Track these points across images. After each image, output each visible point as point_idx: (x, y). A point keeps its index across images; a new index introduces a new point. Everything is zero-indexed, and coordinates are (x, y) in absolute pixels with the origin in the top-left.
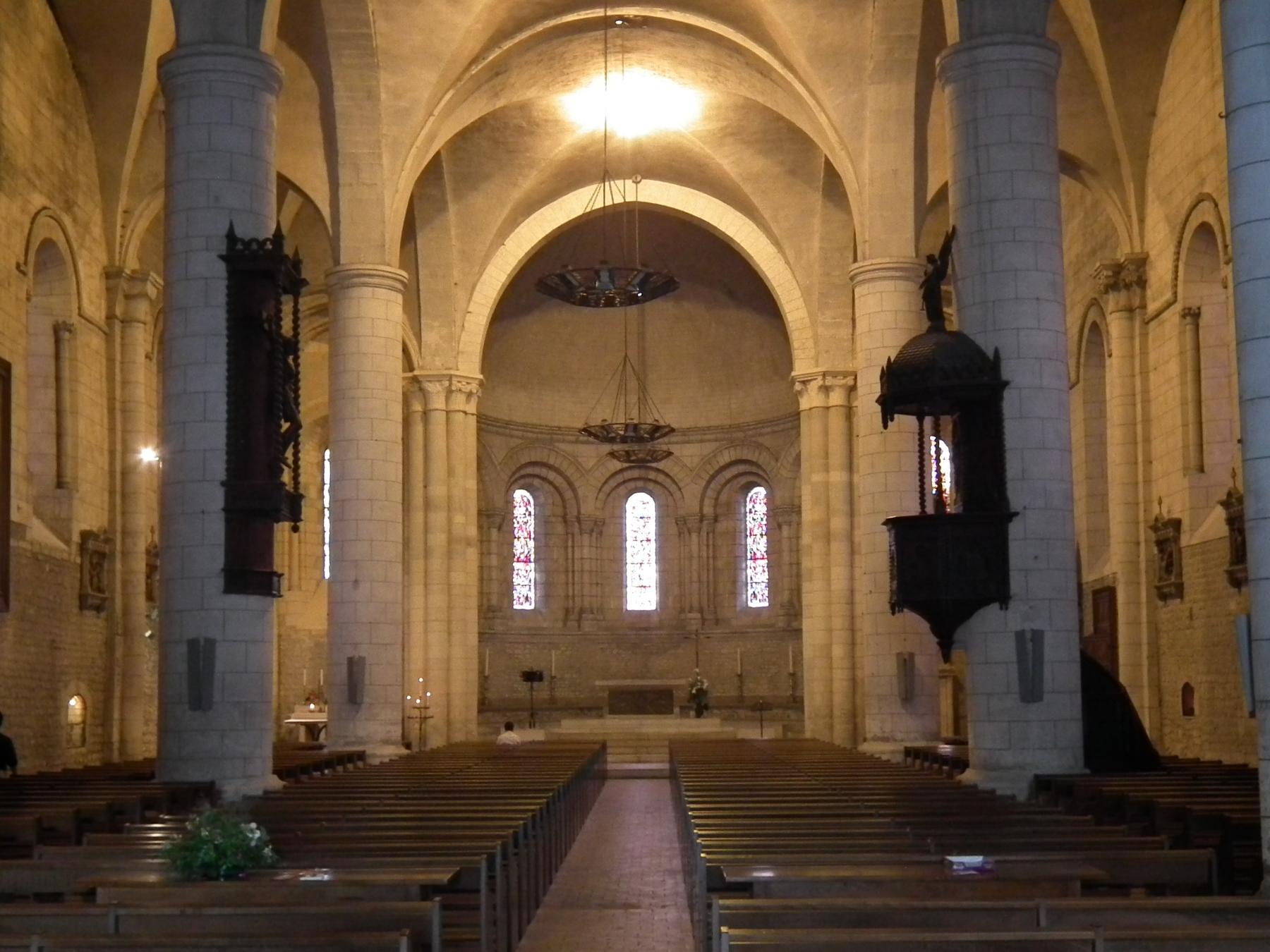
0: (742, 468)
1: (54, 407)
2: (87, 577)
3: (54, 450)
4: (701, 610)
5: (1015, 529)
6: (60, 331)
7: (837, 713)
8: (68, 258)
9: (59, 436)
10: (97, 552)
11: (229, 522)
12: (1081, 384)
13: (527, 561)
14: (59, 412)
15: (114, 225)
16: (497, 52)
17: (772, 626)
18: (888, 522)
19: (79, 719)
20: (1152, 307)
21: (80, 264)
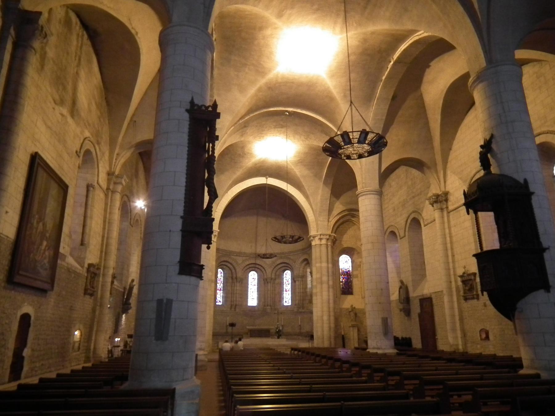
0: (285, 265)
1: (83, 214)
2: (89, 281)
3: (81, 231)
4: (270, 306)
5: (546, 255)
6: (89, 187)
7: (325, 337)
8: (95, 160)
9: (84, 226)
10: (93, 272)
11: (183, 237)
12: (407, 237)
13: (221, 290)
14: (85, 217)
15: (113, 158)
16: (248, 117)
17: (293, 311)
18: (474, 255)
19: (78, 340)
20: (451, 208)
21: (100, 165)
